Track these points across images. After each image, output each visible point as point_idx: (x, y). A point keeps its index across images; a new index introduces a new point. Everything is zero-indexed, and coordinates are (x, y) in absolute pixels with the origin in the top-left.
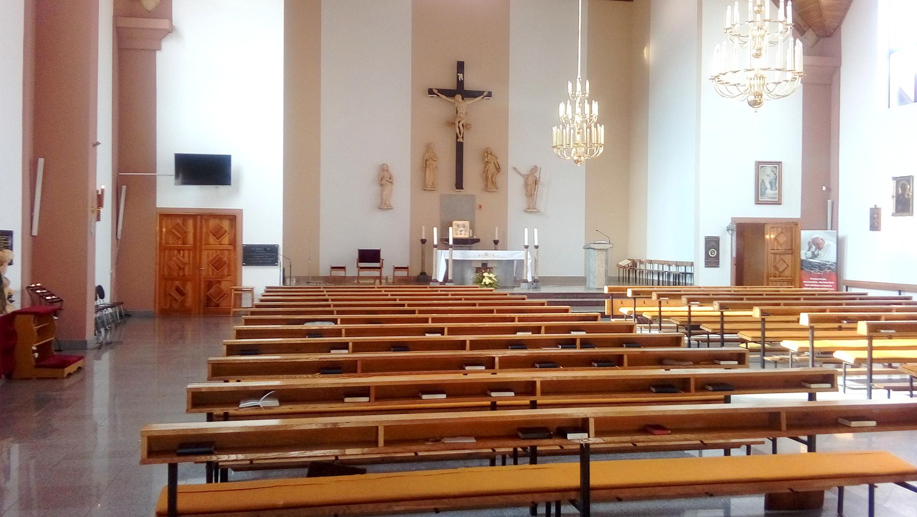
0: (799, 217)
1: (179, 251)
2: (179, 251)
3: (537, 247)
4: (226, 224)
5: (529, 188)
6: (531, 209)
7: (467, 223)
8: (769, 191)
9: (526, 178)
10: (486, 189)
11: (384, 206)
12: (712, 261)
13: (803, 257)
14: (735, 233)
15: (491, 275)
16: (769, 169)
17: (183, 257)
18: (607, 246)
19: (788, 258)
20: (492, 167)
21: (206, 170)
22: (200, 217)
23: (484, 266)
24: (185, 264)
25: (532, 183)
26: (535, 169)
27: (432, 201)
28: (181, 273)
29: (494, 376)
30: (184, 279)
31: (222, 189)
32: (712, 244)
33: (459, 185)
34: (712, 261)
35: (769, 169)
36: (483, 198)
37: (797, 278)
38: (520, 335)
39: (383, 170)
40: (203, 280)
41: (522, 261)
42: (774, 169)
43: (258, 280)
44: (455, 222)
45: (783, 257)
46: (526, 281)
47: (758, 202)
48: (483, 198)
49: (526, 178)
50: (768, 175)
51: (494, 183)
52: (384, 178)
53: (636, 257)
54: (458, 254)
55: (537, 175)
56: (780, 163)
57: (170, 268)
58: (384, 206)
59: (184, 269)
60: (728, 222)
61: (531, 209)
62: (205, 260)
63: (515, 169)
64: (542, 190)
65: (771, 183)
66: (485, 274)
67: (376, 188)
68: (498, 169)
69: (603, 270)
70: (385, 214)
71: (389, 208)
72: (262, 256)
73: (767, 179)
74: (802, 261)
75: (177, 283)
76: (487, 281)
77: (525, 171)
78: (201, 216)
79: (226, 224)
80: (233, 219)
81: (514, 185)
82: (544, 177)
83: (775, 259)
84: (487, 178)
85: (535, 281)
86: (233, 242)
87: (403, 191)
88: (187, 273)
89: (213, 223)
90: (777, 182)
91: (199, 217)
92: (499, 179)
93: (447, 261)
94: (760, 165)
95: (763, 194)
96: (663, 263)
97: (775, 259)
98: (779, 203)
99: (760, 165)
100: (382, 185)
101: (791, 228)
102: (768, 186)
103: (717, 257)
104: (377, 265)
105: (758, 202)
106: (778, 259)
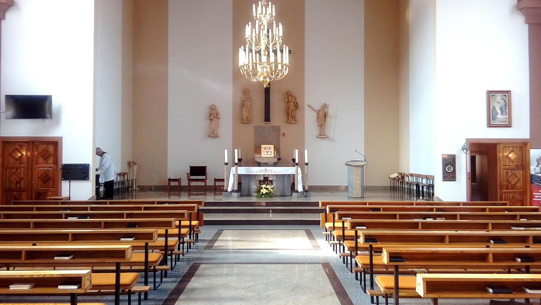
0: (528, 137)
1: (17, 169)
2: (17, 169)
3: (307, 164)
4: (51, 149)
5: (320, 120)
6: (322, 135)
7: (272, 146)
8: (499, 116)
9: (318, 112)
10: (288, 122)
11: (213, 135)
12: (450, 175)
13: (533, 172)
14: (468, 152)
15: (268, 186)
16: (499, 97)
17: (20, 174)
18: (362, 164)
19: (519, 173)
20: (292, 104)
21: (32, 107)
22: (32, 143)
23: (266, 180)
24: (21, 179)
25: (323, 116)
26: (325, 106)
27: (249, 131)
28: (18, 186)
29: (487, 233)
30: (20, 190)
31: (47, 121)
32: (449, 162)
33: (267, 119)
34: (450, 175)
35: (499, 97)
36: (285, 128)
37: (528, 190)
38: (439, 220)
39: (212, 109)
40: (34, 191)
41: (294, 175)
42: (504, 98)
43: (81, 191)
44: (263, 146)
45: (514, 172)
46: (297, 192)
47: (490, 125)
48: (285, 128)
49: (318, 112)
50: (498, 102)
51: (294, 118)
52: (213, 115)
53: (404, 171)
54: (242, 170)
55: (326, 110)
56: (510, 91)
57: (10, 182)
58: (213, 135)
59: (20, 183)
60: (463, 142)
61: (322, 135)
62: (35, 176)
63: (309, 106)
64: (331, 122)
65: (501, 109)
66: (263, 186)
67: (208, 122)
68: (296, 106)
69: (359, 182)
70: (214, 141)
71: (216, 136)
72: (78, 172)
73: (498, 103)
74: (532, 176)
75: (15, 193)
76: (264, 191)
77: (317, 107)
78: (33, 142)
79: (51, 149)
80: (55, 145)
81: (309, 119)
82: (331, 111)
83: (507, 173)
84: (288, 114)
85: (305, 191)
86: (56, 162)
87: (227, 124)
88: (22, 186)
89: (42, 147)
90: (507, 108)
91: (31, 143)
92: (298, 114)
93: (234, 175)
94: (491, 94)
95: (494, 118)
96: (419, 176)
97: (507, 173)
98: (509, 126)
99: (491, 94)
100: (211, 120)
101: (522, 147)
102: (499, 111)
103: (454, 172)
104: (203, 177)
105: (490, 125)
106: (510, 174)
